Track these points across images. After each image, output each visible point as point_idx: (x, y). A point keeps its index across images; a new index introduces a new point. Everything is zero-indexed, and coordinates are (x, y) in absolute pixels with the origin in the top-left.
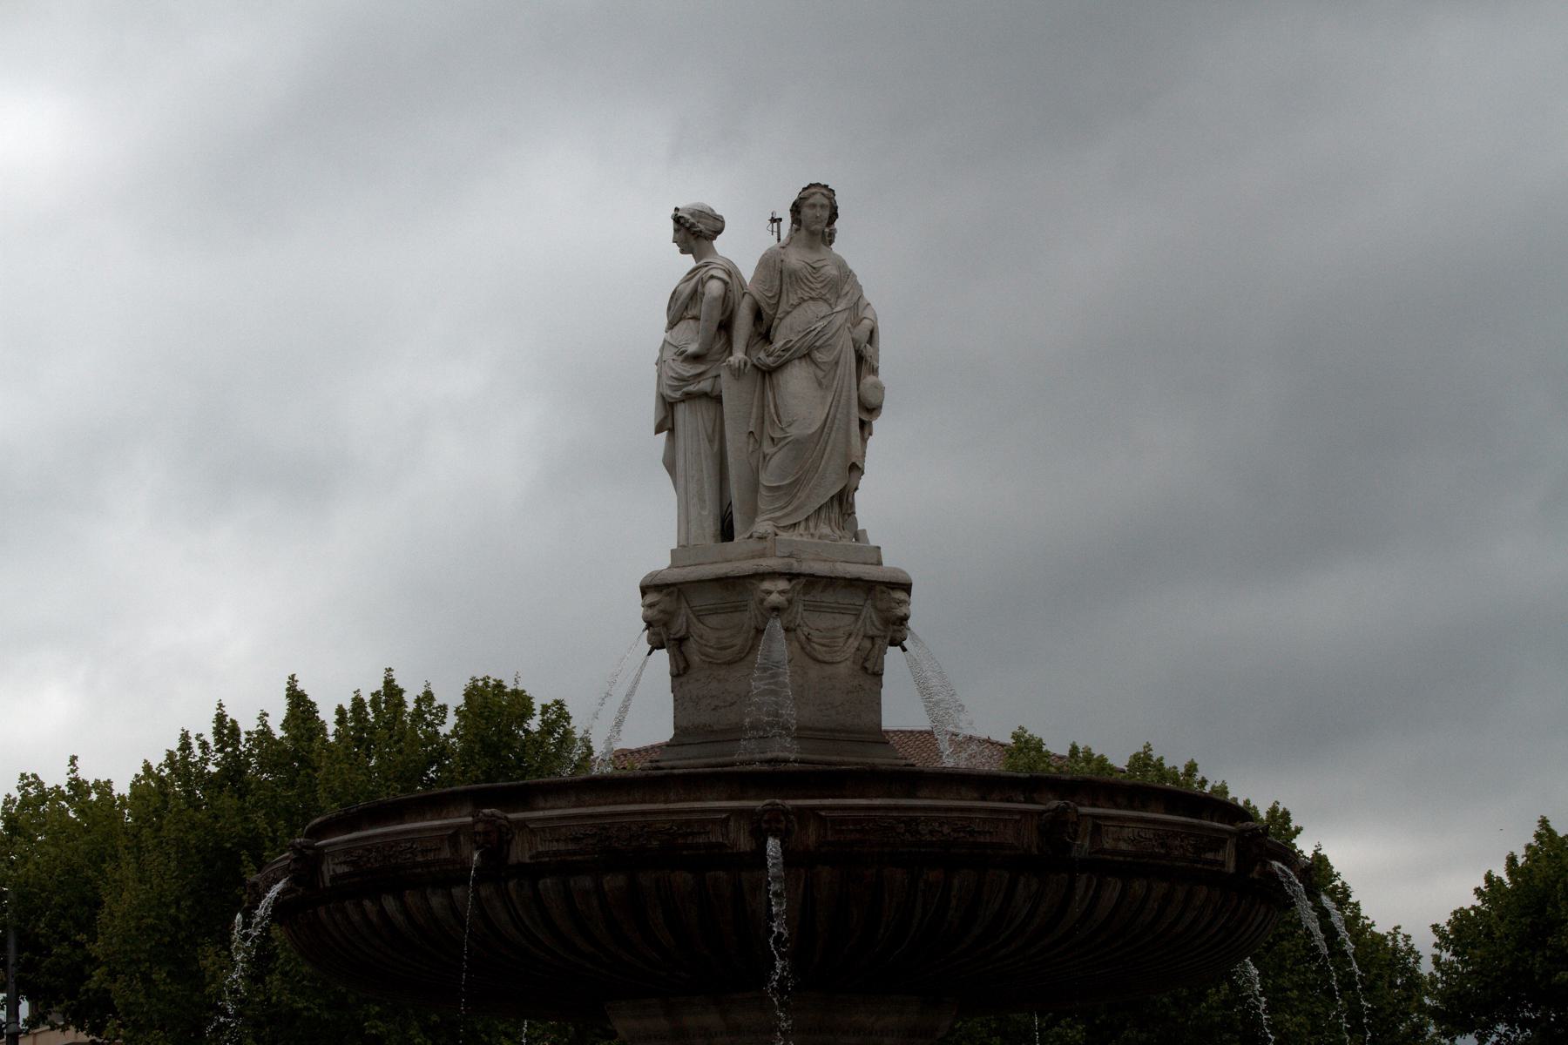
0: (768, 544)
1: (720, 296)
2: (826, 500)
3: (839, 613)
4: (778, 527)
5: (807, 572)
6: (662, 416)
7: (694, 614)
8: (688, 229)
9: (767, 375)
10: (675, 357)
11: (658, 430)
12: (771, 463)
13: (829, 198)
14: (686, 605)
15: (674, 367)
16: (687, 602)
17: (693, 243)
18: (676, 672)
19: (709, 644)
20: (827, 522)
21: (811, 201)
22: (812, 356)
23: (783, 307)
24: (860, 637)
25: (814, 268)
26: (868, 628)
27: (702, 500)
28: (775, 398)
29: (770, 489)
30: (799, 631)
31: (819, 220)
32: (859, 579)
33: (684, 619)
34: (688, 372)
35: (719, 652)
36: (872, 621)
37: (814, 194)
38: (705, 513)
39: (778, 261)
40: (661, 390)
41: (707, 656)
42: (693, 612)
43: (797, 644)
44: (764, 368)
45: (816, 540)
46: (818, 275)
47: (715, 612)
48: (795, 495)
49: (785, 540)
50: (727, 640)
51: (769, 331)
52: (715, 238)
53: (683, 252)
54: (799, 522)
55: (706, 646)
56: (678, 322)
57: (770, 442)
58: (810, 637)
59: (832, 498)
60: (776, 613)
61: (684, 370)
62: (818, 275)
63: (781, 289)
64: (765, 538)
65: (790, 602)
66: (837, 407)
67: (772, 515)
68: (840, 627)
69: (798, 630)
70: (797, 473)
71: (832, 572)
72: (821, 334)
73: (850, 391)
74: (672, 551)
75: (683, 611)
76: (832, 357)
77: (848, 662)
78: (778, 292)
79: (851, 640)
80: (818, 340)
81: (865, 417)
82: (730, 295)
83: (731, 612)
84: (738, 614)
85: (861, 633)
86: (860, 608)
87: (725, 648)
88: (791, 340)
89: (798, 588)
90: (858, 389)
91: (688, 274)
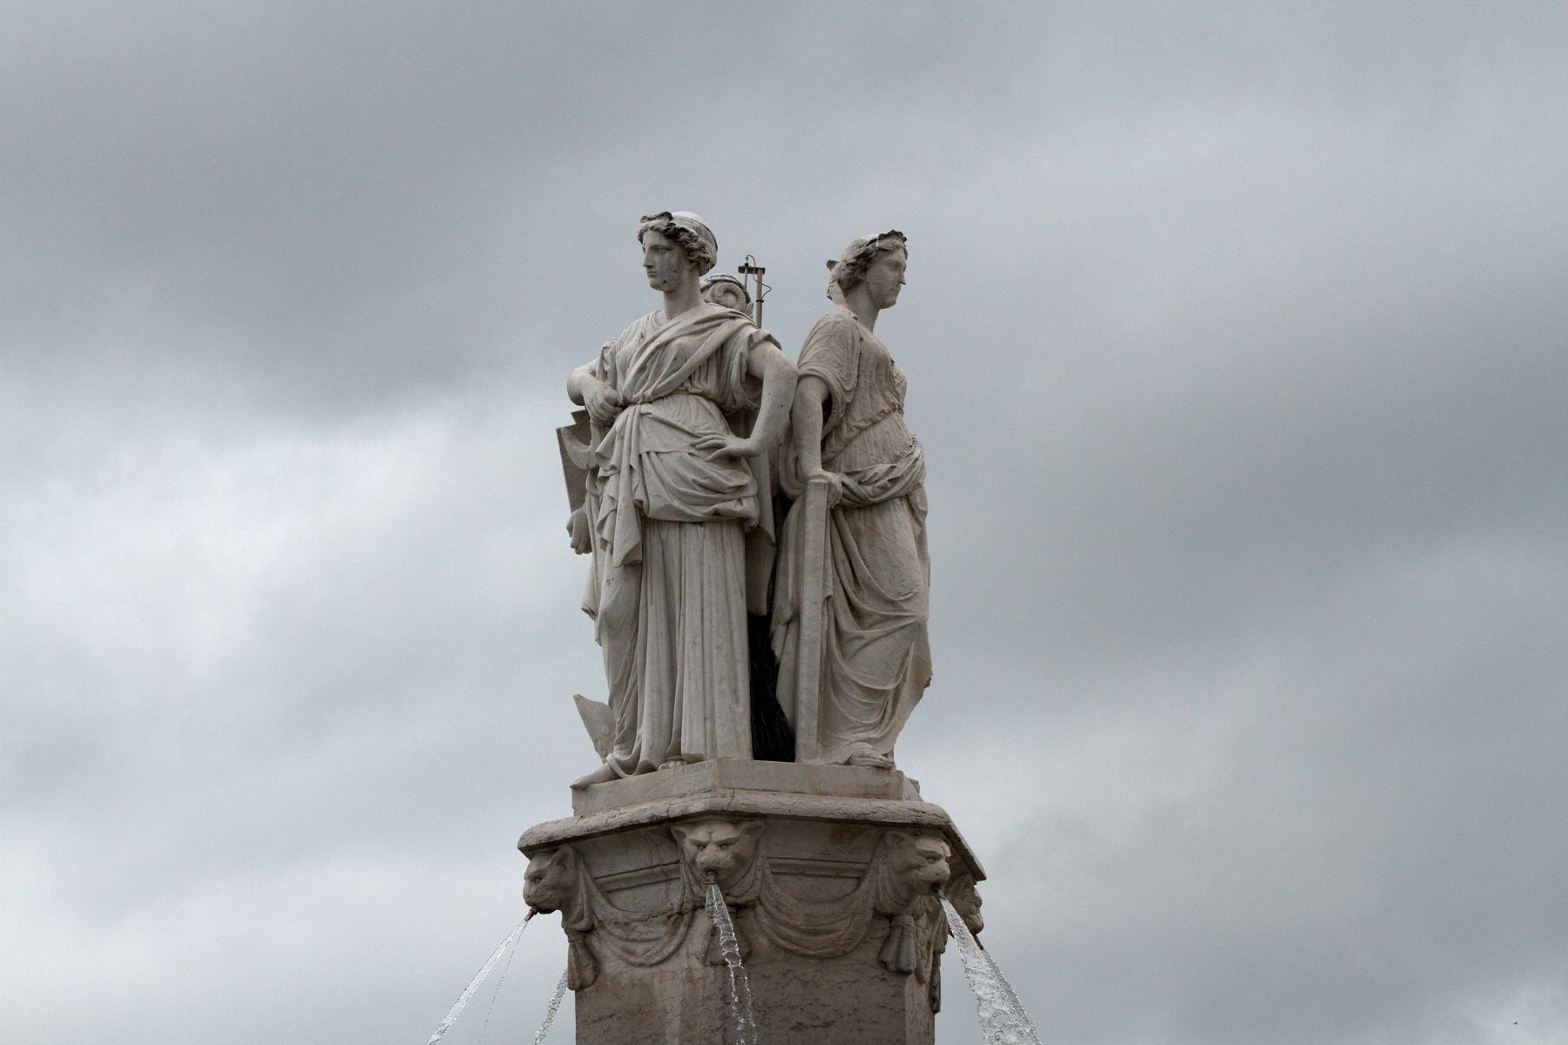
40: (640, 495)
55: (786, 924)
83: (830, 877)
87: (816, 933)
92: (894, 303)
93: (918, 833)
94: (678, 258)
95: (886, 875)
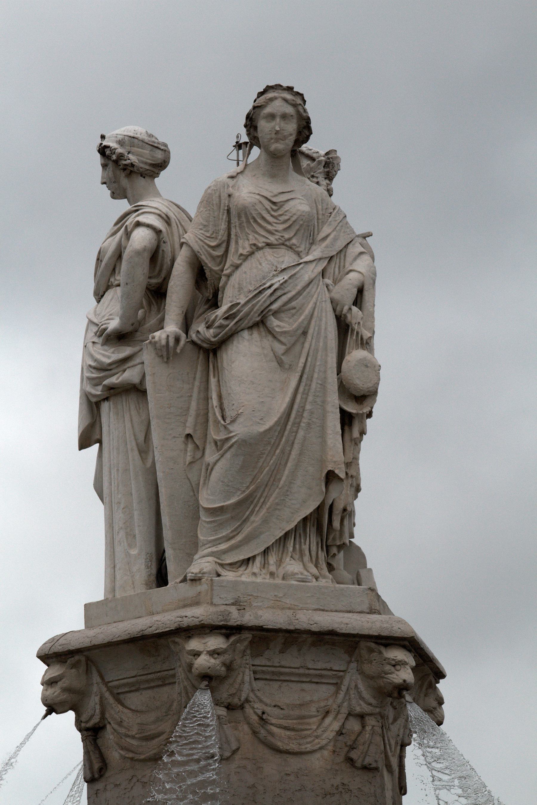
0: (203, 587)
1: (144, 249)
2: (292, 525)
3: (310, 682)
4: (222, 565)
5: (250, 624)
6: (87, 422)
7: (112, 693)
8: (116, 162)
9: (211, 355)
10: (96, 339)
11: (84, 443)
12: (214, 472)
13: (295, 105)
14: (99, 680)
15: (93, 352)
16: (102, 677)
17: (124, 182)
18: (89, 776)
19: (130, 733)
20: (297, 556)
21: (268, 110)
22: (268, 324)
23: (232, 259)
24: (342, 717)
25: (274, 203)
26: (354, 702)
27: (130, 535)
28: (219, 386)
29: (212, 512)
30: (248, 710)
31: (280, 136)
32: (332, 633)
33: (97, 699)
34: (109, 357)
35: (144, 743)
36: (359, 693)
37: (271, 100)
38: (134, 552)
39: (224, 196)
41: (128, 750)
42: (110, 690)
43: (246, 728)
44: (205, 345)
45: (278, 581)
46: (280, 212)
47: (135, 688)
48: (247, 518)
49: (228, 582)
50: (153, 727)
51: (216, 294)
52: (158, 175)
53: (114, 196)
54: (254, 557)
55: (127, 736)
56: (104, 293)
57: (214, 448)
58: (264, 717)
59: (305, 520)
60: (206, 683)
61: (104, 355)
62: (280, 212)
63: (229, 235)
64: (200, 579)
65: (229, 667)
66: (306, 394)
67: (214, 549)
68: (312, 701)
69: (247, 706)
70: (248, 487)
71: (289, 624)
72: (279, 293)
73: (325, 372)
74: (440, 675)
75: (95, 689)
76: (295, 326)
77: (326, 753)
78: (225, 238)
79: (328, 720)
80: (276, 300)
81: (351, 408)
82: (163, 247)
83: (158, 686)
84: (166, 689)
85: (344, 710)
86: (341, 674)
88: (239, 304)
89: (240, 647)
90: (339, 371)
91: (116, 224)
92: (158, 177)
93: (190, 635)
94: (113, 171)
95: (183, 676)
